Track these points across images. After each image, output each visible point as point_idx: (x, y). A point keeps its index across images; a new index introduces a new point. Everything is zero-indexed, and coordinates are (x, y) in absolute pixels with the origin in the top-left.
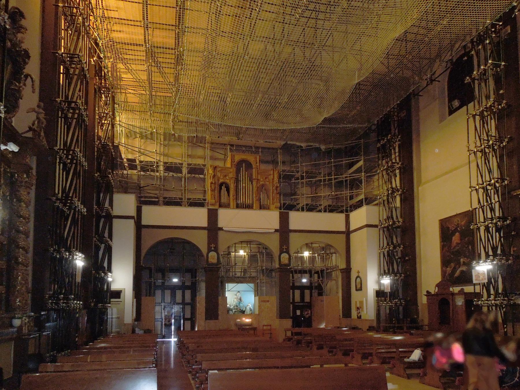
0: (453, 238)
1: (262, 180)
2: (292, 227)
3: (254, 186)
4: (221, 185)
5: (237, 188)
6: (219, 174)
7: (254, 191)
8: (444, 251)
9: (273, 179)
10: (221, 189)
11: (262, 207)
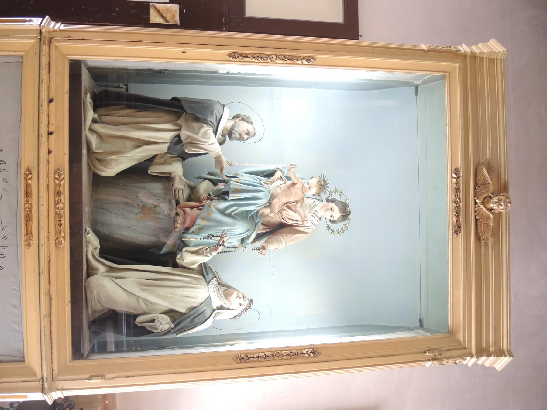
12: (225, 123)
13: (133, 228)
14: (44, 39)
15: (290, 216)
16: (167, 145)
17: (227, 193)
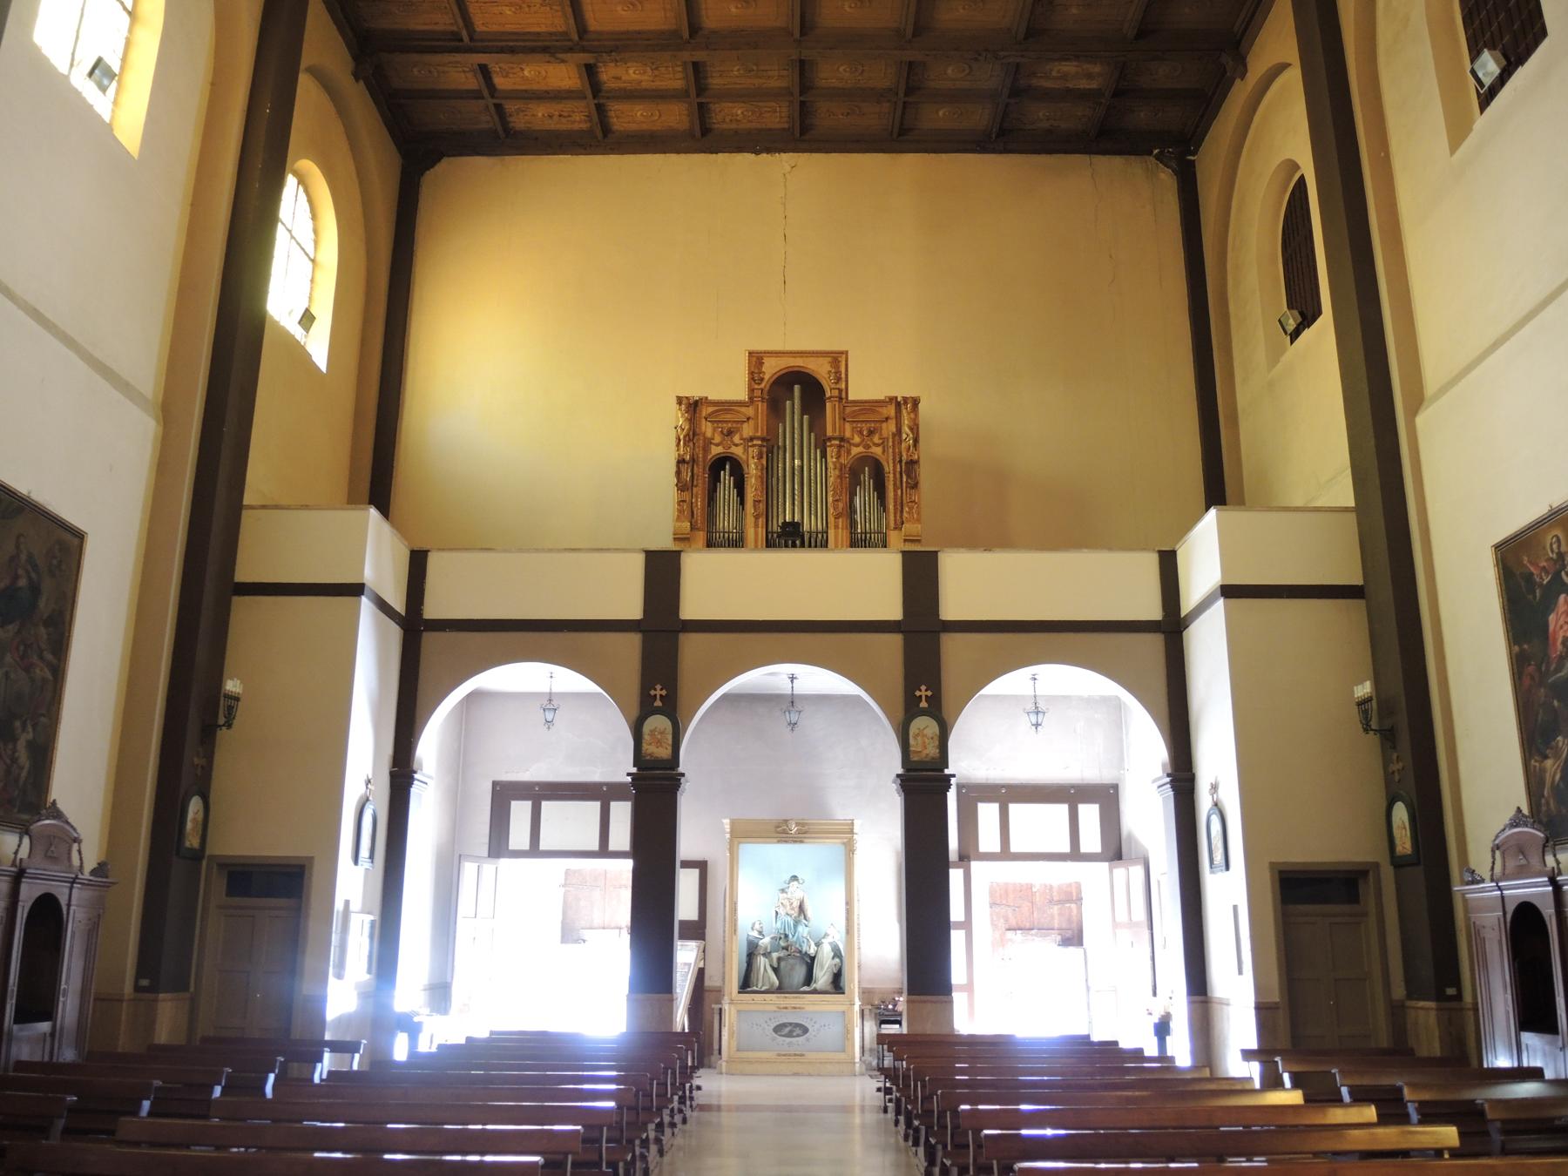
0: (1552, 618)
1: (857, 439)
2: (691, 609)
3: (830, 465)
4: (719, 464)
5: (768, 472)
6: (707, 429)
7: (831, 480)
8: (1527, 681)
9: (899, 431)
10: (715, 479)
11: (858, 541)
12: (755, 934)
13: (799, 973)
14: (732, 1002)
15: (796, 904)
16: (1151, 1050)
17: (842, 439)
